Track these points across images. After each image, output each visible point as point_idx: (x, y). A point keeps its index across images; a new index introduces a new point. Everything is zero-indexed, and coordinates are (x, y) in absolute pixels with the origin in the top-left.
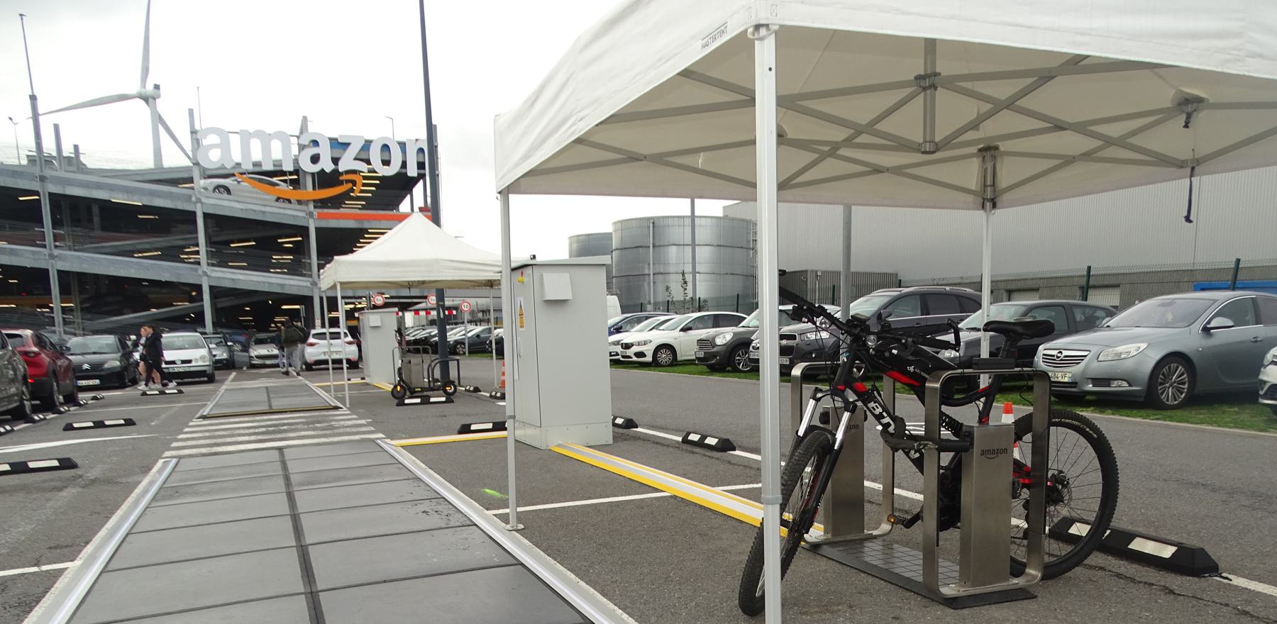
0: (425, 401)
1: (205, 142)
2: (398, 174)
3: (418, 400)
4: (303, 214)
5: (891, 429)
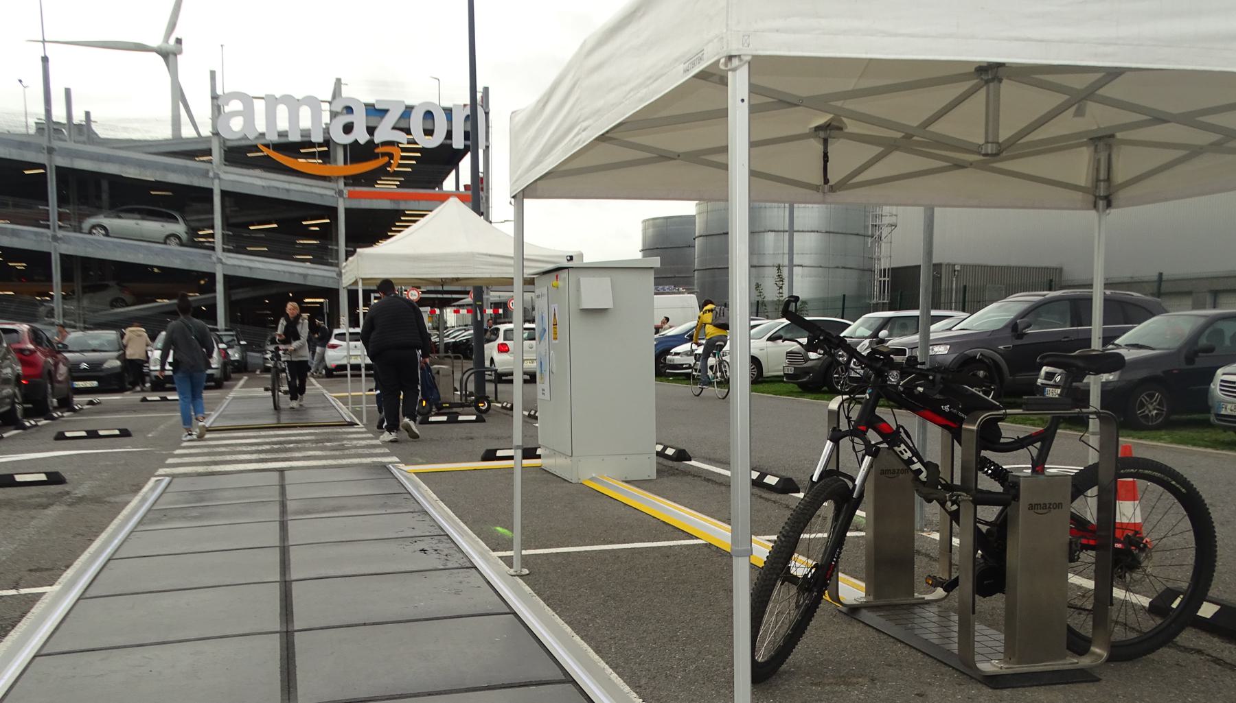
0: (453, 419)
1: (227, 109)
2: (441, 145)
3: (444, 418)
4: (332, 193)
5: (923, 476)
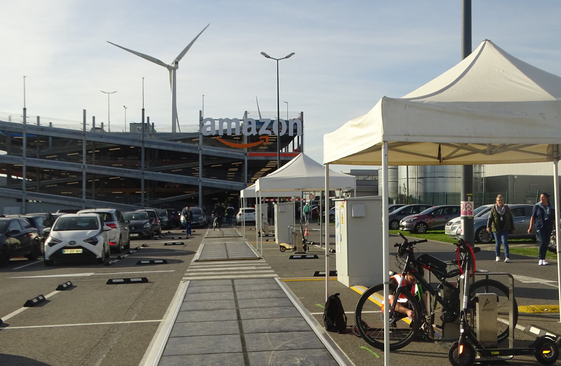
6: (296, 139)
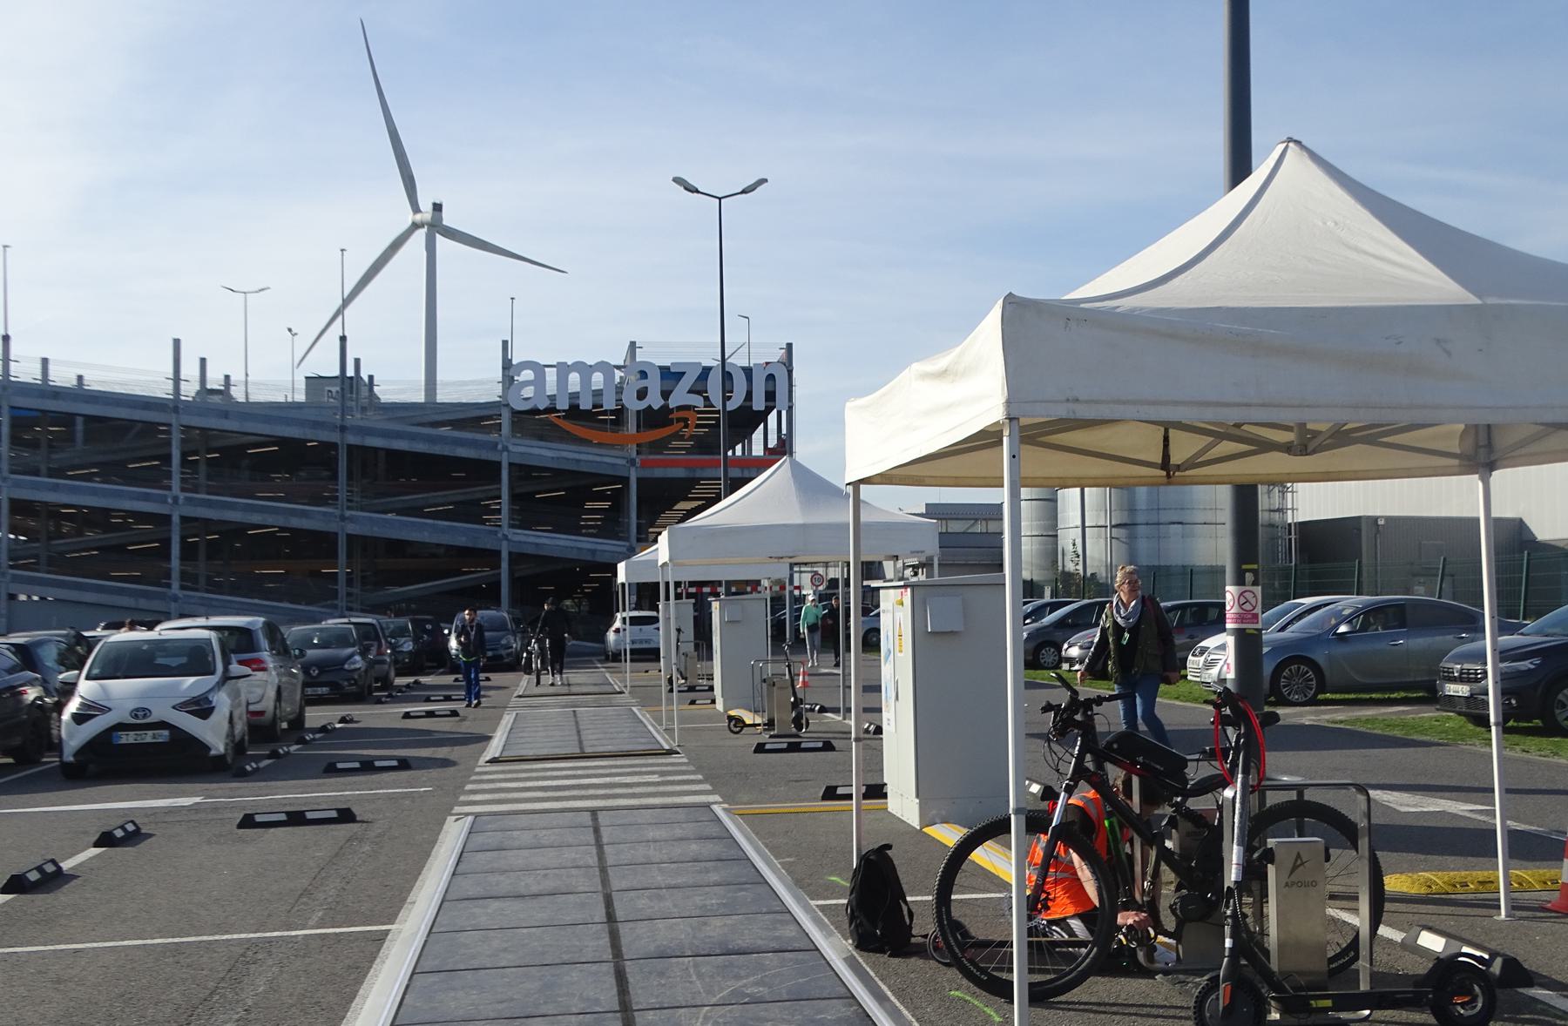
4: (623, 462)
6: (772, 418)
